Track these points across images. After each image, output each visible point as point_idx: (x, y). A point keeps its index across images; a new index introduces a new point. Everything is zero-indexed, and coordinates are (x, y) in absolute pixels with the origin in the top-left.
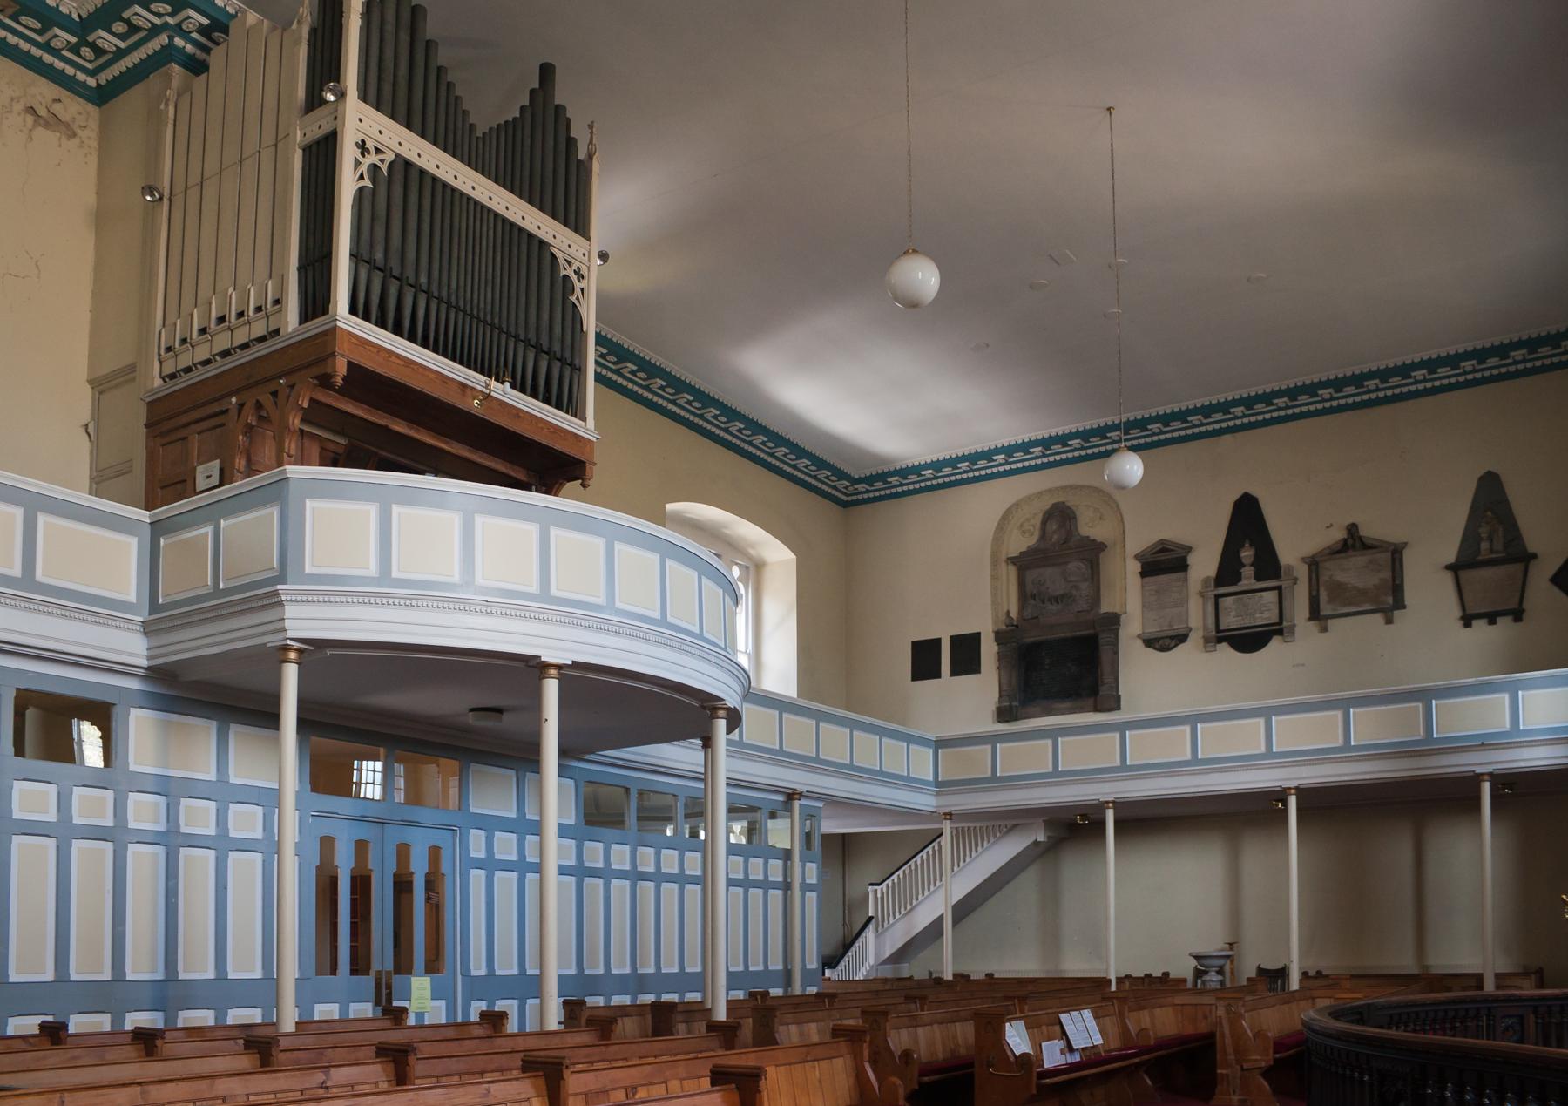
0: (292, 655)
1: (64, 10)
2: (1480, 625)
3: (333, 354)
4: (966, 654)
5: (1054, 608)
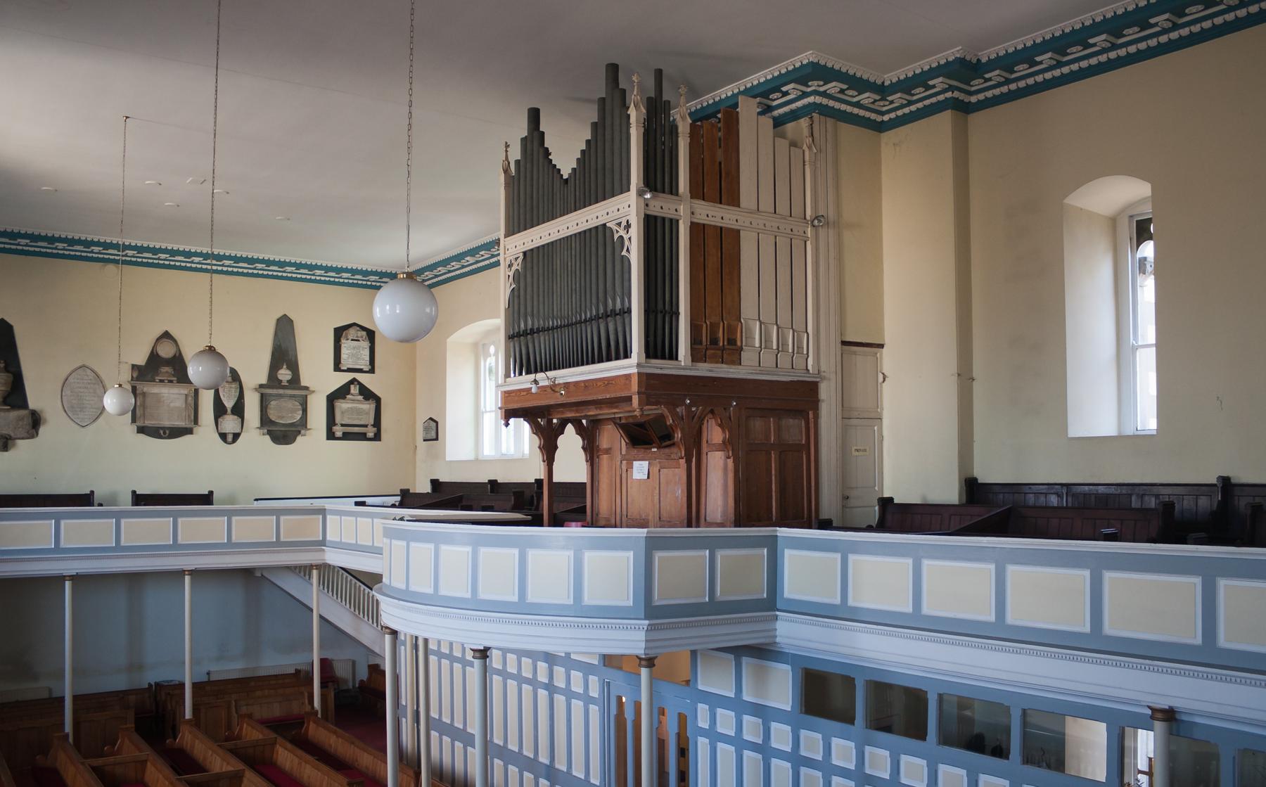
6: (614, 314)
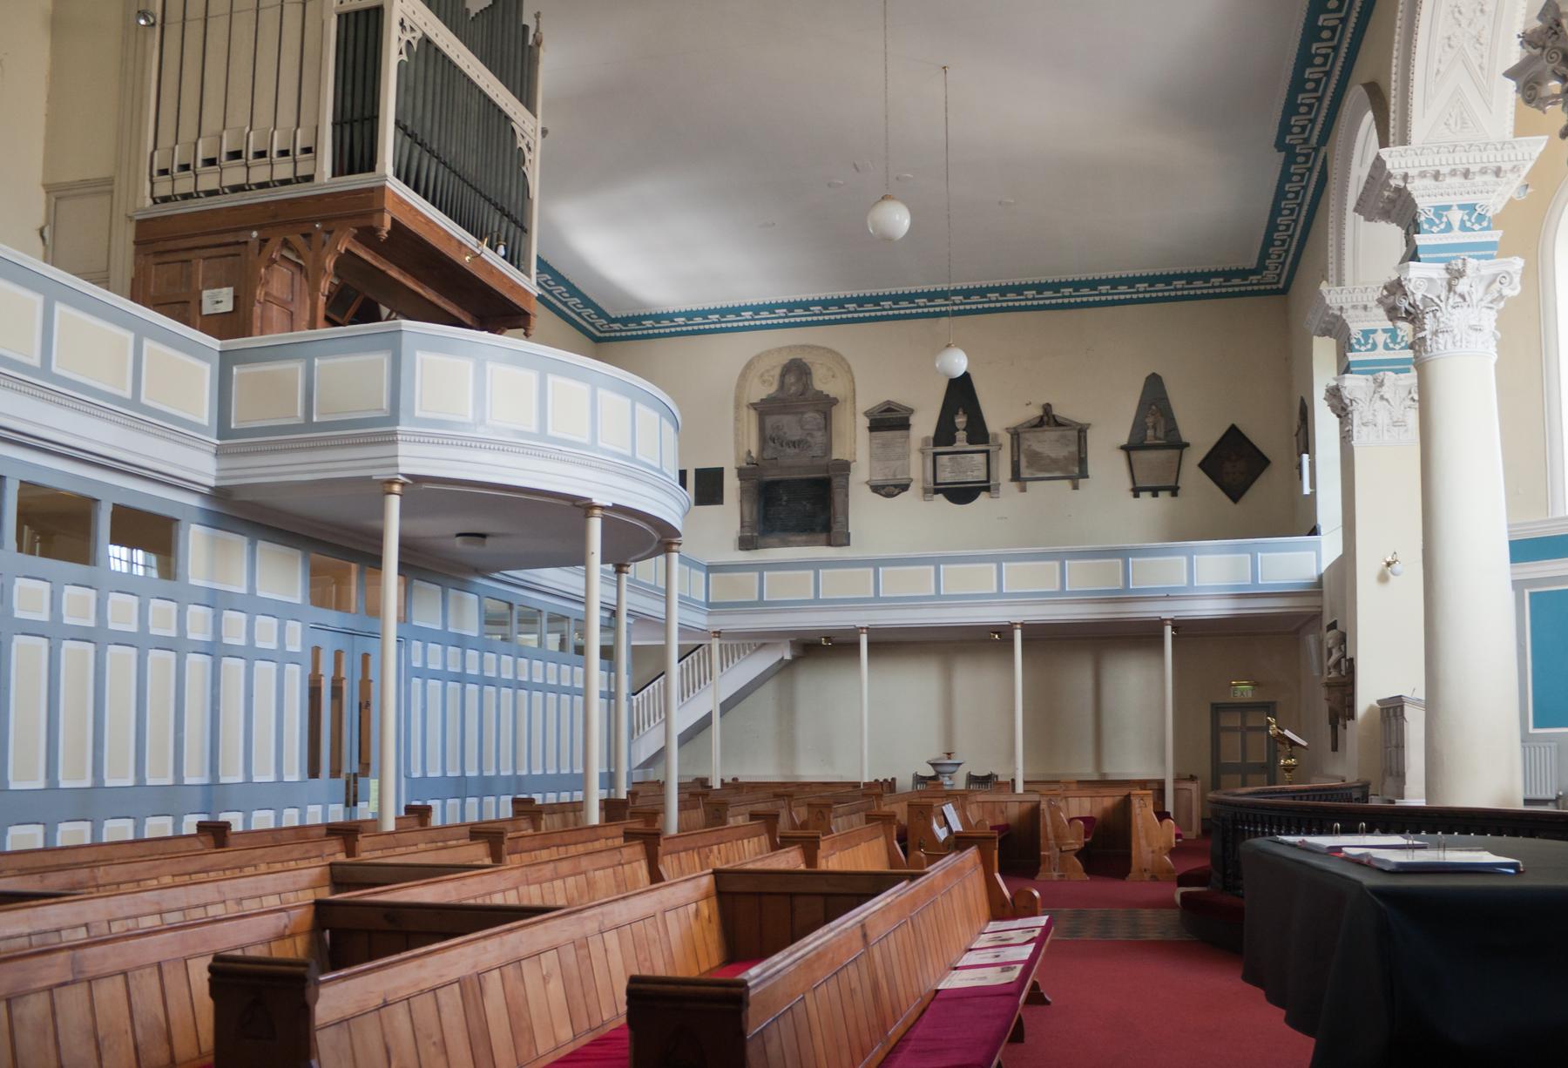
0: (396, 488)
2: (1146, 496)
3: (382, 210)
5: (791, 451)
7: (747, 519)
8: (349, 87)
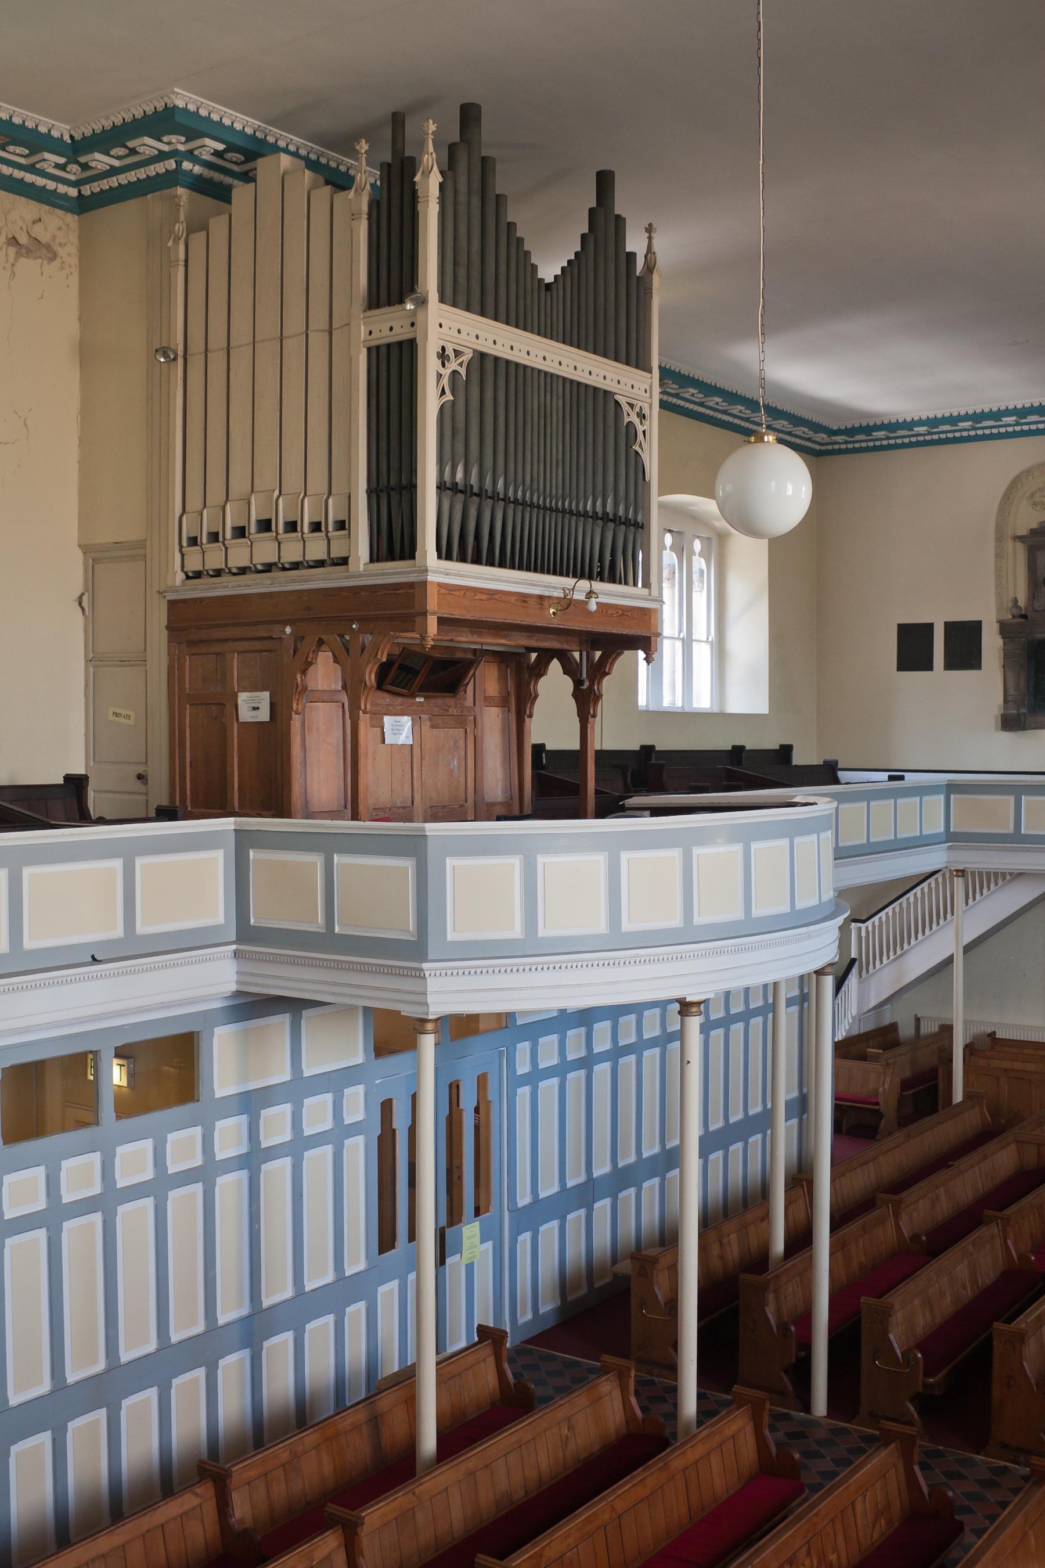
0: (430, 1026)
1: (55, 134)
3: (424, 614)
4: (964, 646)
6: (627, 523)
7: (1012, 692)
8: (383, 445)
